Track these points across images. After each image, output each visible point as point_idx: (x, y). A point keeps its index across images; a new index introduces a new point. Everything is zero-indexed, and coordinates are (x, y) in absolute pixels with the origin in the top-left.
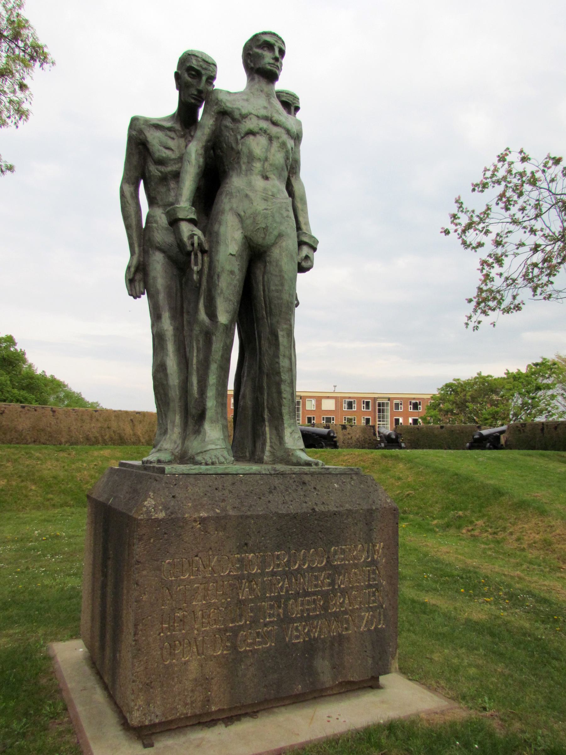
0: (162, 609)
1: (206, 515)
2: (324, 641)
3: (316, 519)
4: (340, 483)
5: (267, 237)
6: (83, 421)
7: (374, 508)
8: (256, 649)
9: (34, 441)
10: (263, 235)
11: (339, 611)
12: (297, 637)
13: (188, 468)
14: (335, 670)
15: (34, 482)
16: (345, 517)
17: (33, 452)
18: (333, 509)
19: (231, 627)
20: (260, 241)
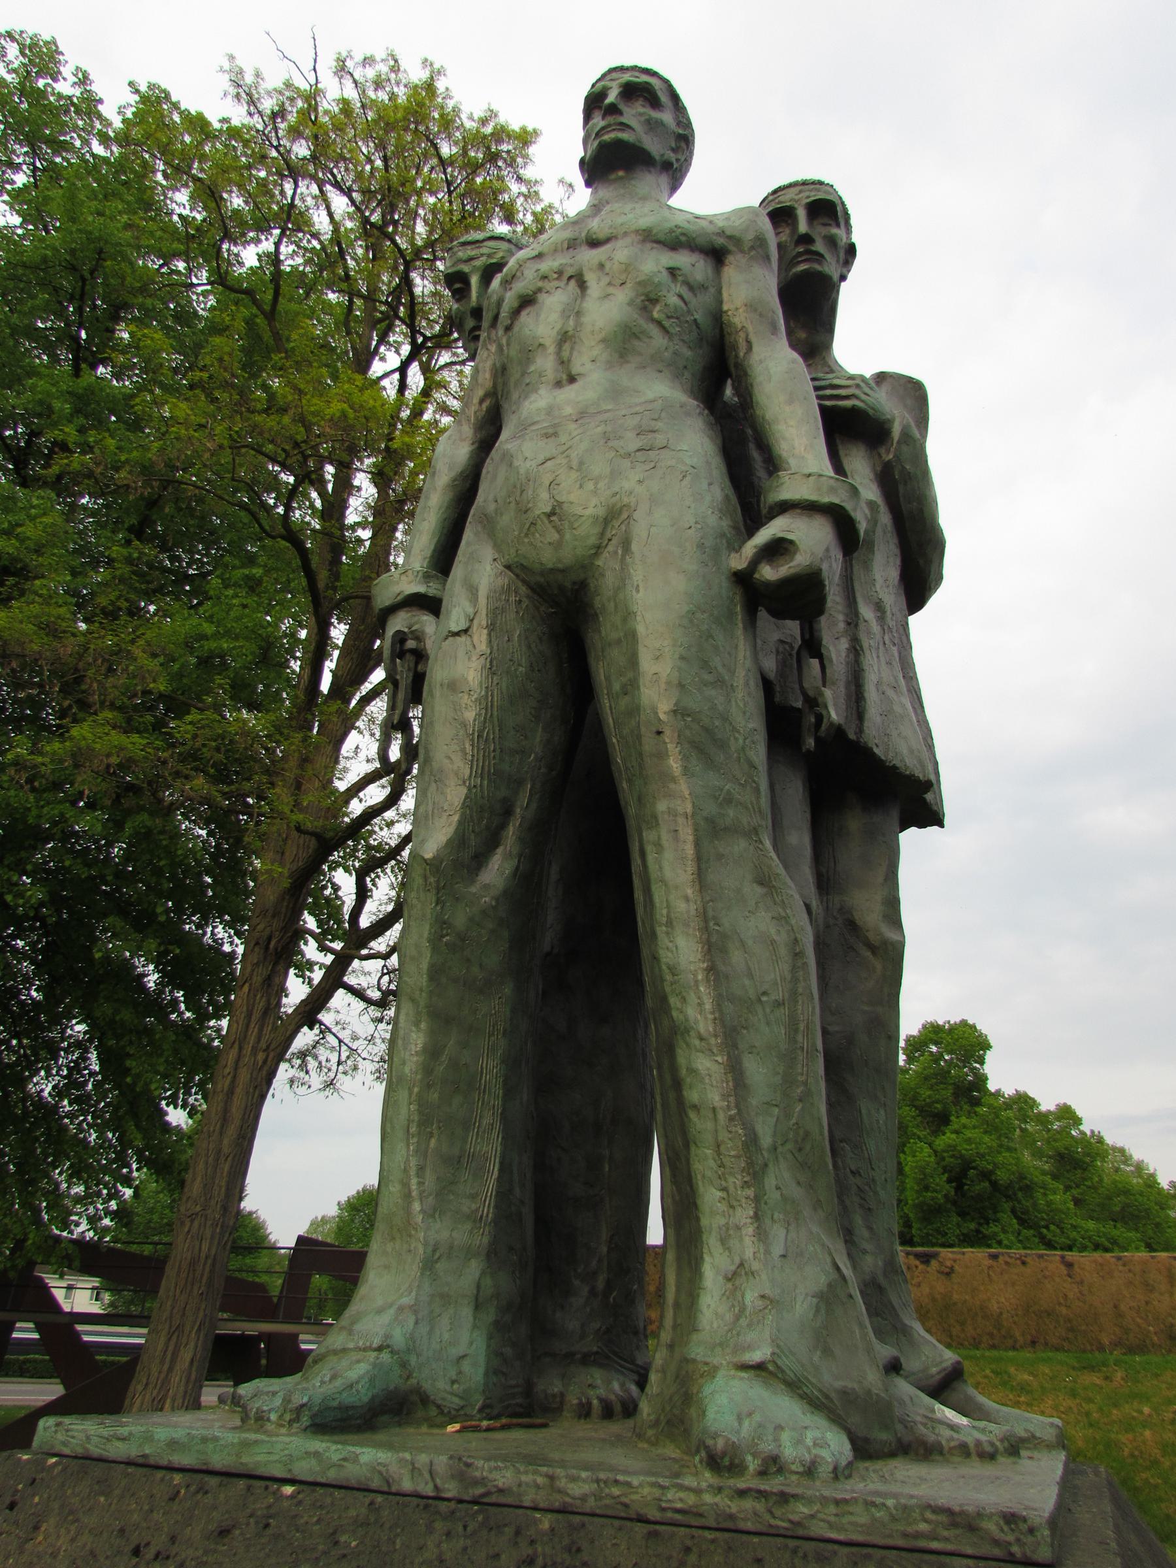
5: (568, 536)
6: (1149, 1287)
10: (554, 536)
13: (105, 1432)
17: (1012, 1370)
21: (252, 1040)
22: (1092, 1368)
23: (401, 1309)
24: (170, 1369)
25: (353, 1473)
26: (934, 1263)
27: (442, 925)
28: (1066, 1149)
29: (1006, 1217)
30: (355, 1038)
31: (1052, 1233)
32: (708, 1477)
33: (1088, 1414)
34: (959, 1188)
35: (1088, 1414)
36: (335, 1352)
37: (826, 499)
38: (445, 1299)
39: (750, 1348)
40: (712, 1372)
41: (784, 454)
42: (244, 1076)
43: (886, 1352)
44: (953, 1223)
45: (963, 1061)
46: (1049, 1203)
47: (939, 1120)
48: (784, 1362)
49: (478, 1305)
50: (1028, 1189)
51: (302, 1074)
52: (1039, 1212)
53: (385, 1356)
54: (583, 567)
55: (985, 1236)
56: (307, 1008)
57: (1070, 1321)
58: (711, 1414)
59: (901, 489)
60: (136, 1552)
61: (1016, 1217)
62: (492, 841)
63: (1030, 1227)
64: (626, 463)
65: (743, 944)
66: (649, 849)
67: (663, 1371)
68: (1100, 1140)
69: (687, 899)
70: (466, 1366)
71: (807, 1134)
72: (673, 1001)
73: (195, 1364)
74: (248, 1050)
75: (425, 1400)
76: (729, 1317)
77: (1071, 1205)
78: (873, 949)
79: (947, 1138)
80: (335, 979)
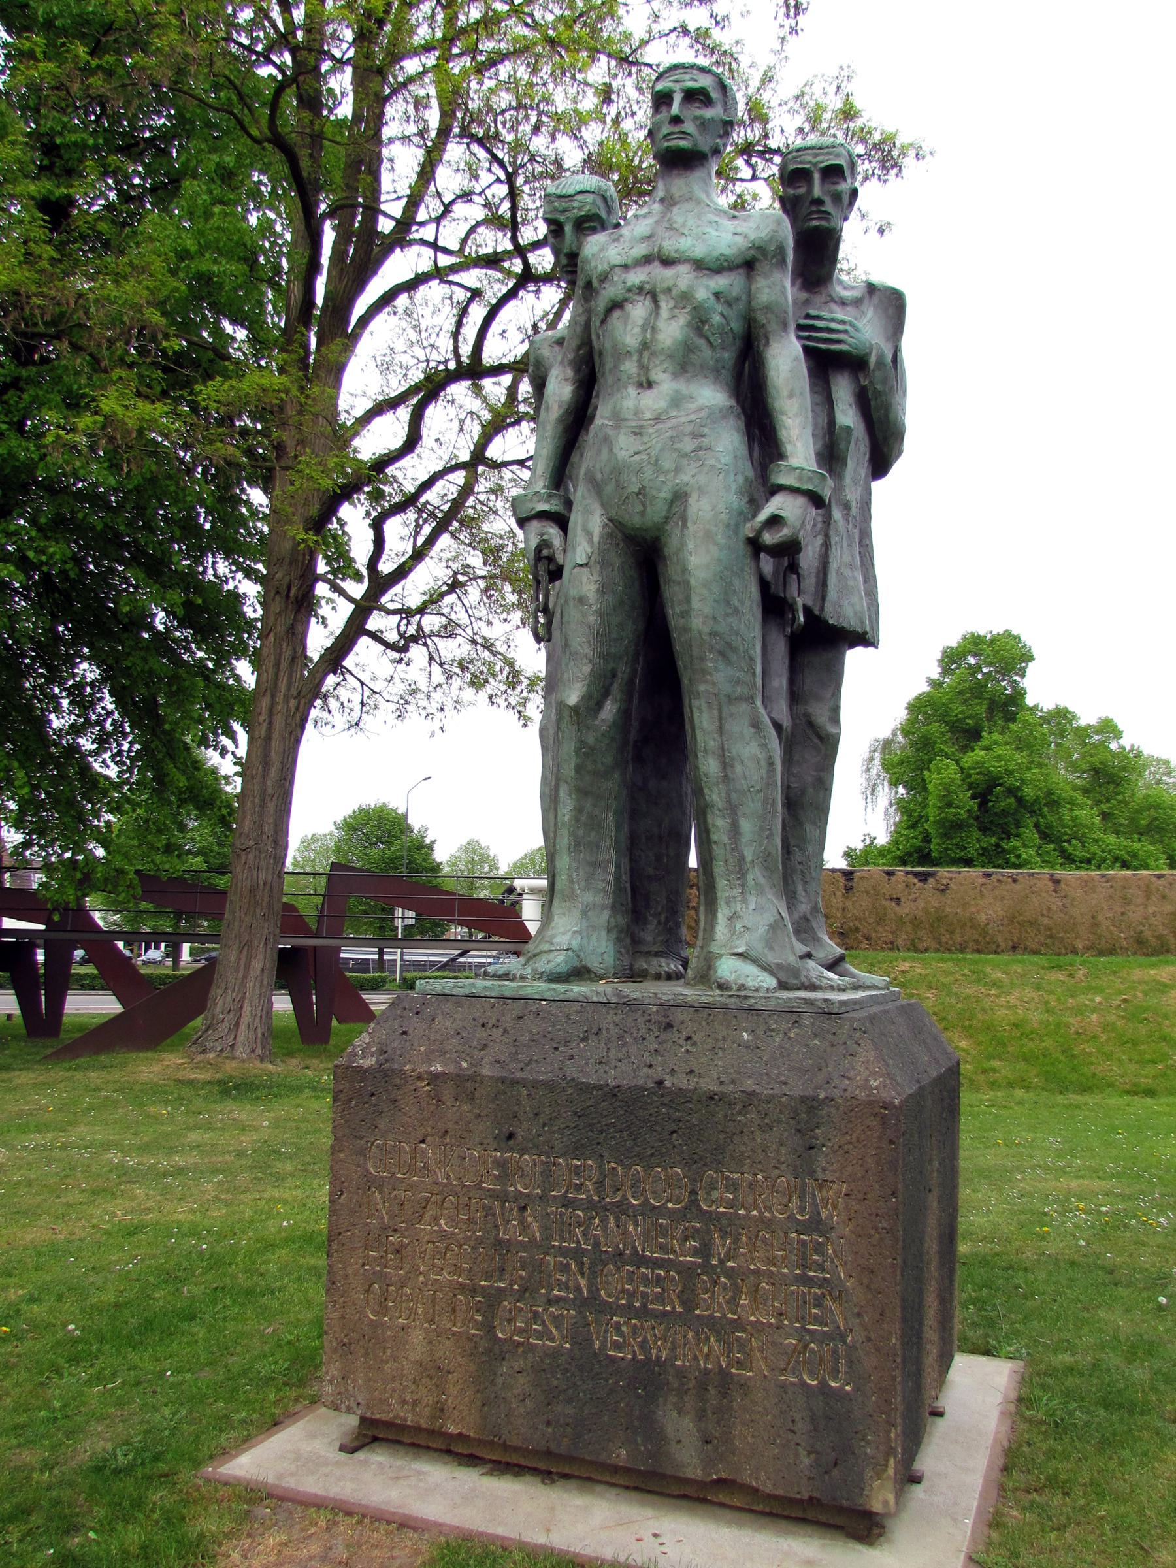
0: (367, 1224)
1: (440, 1069)
2: (681, 1373)
3: (664, 1105)
4: (760, 1032)
5: (649, 509)
6: (1126, 901)
7: (822, 1096)
8: (531, 1344)
9: (1014, 948)
10: (639, 508)
11: (720, 1318)
12: (618, 1346)
14: (709, 1446)
15: (968, 1032)
16: (738, 1107)
17: (988, 969)
18: (708, 1084)
19: (483, 1287)
20: (637, 521)
21: (283, 687)
22: (1059, 967)
23: (575, 932)
24: (245, 977)
25: (571, 996)
26: (931, 880)
27: (582, 743)
28: (1101, 763)
29: (1030, 834)
30: (374, 678)
31: (1072, 848)
32: (718, 992)
33: (1047, 1003)
34: (983, 804)
35: (1047, 1003)
36: (545, 952)
37: (805, 487)
38: (594, 928)
39: (736, 947)
40: (721, 956)
41: (784, 440)
42: (279, 722)
43: (802, 949)
44: (974, 841)
45: (1003, 675)
46: (1074, 819)
47: (970, 735)
48: (752, 953)
49: (609, 931)
50: (1054, 804)
51: (325, 714)
52: (1063, 826)
53: (570, 953)
54: (658, 529)
55: (1004, 850)
56: (333, 656)
57: (1050, 929)
58: (719, 971)
59: (872, 403)
60: (483, 1025)
61: (1039, 831)
62: (606, 693)
63: (1052, 842)
64: (685, 462)
65: (742, 762)
66: (695, 710)
67: (698, 957)
68: (1139, 755)
69: (714, 740)
70: (605, 957)
71: (769, 854)
72: (706, 791)
73: (266, 972)
74: (280, 698)
75: (588, 971)
76: (729, 935)
77: (1097, 820)
78: (821, 738)
79: (977, 754)
80: (355, 629)
